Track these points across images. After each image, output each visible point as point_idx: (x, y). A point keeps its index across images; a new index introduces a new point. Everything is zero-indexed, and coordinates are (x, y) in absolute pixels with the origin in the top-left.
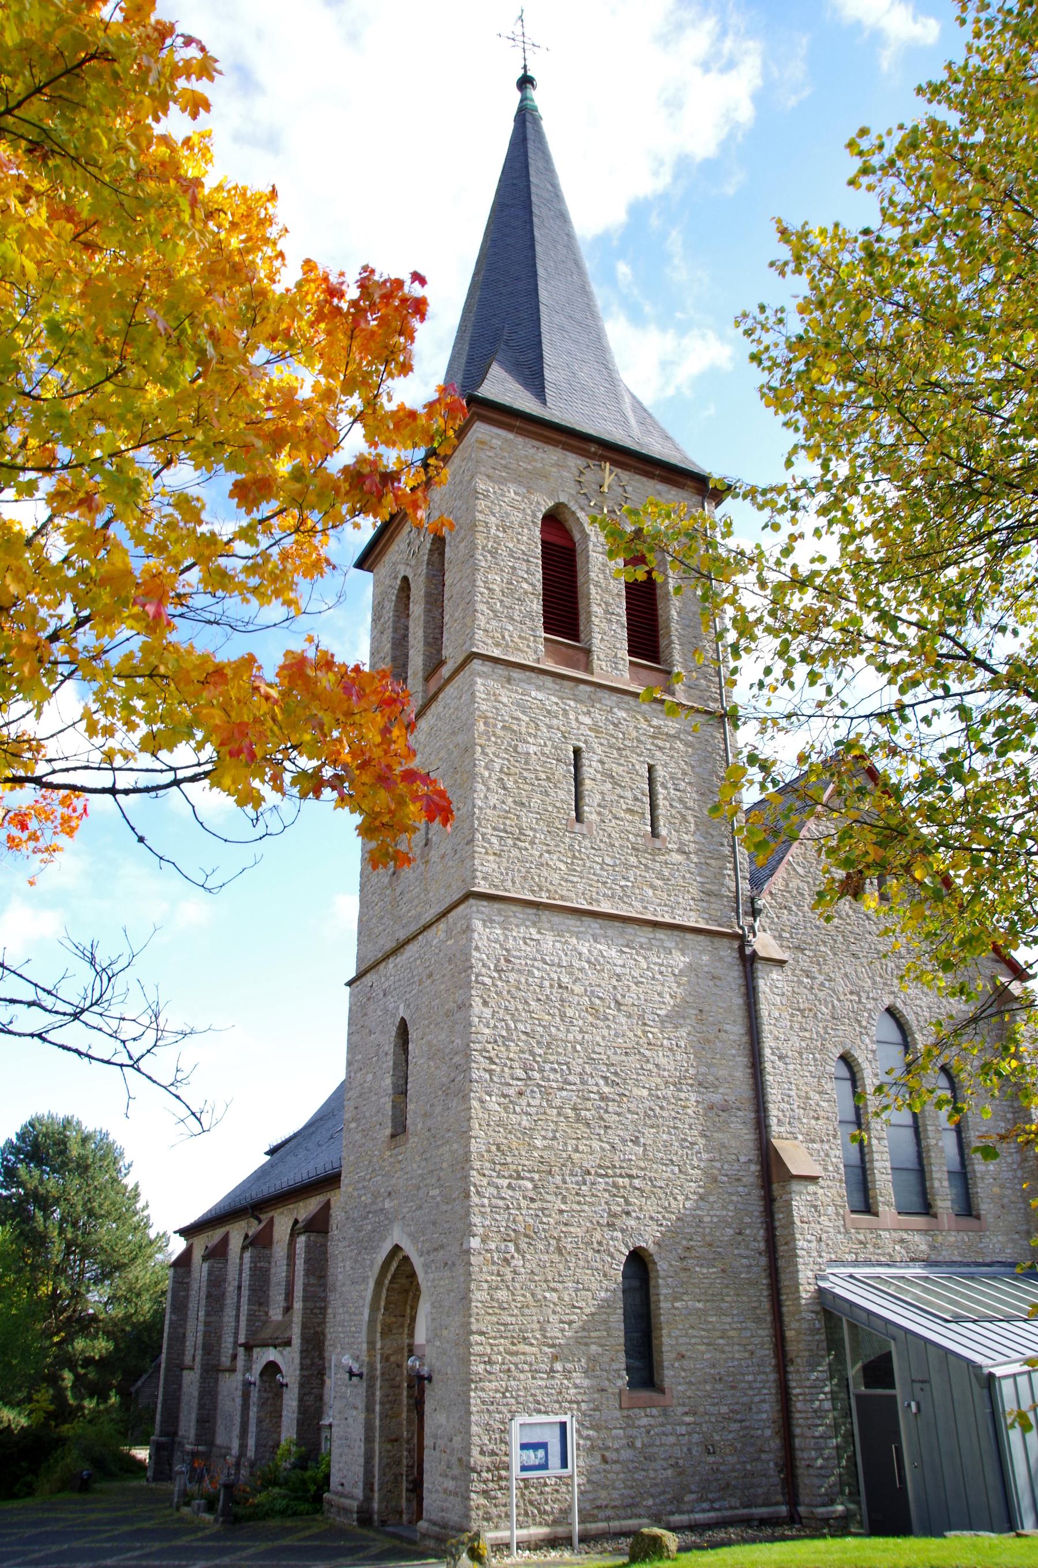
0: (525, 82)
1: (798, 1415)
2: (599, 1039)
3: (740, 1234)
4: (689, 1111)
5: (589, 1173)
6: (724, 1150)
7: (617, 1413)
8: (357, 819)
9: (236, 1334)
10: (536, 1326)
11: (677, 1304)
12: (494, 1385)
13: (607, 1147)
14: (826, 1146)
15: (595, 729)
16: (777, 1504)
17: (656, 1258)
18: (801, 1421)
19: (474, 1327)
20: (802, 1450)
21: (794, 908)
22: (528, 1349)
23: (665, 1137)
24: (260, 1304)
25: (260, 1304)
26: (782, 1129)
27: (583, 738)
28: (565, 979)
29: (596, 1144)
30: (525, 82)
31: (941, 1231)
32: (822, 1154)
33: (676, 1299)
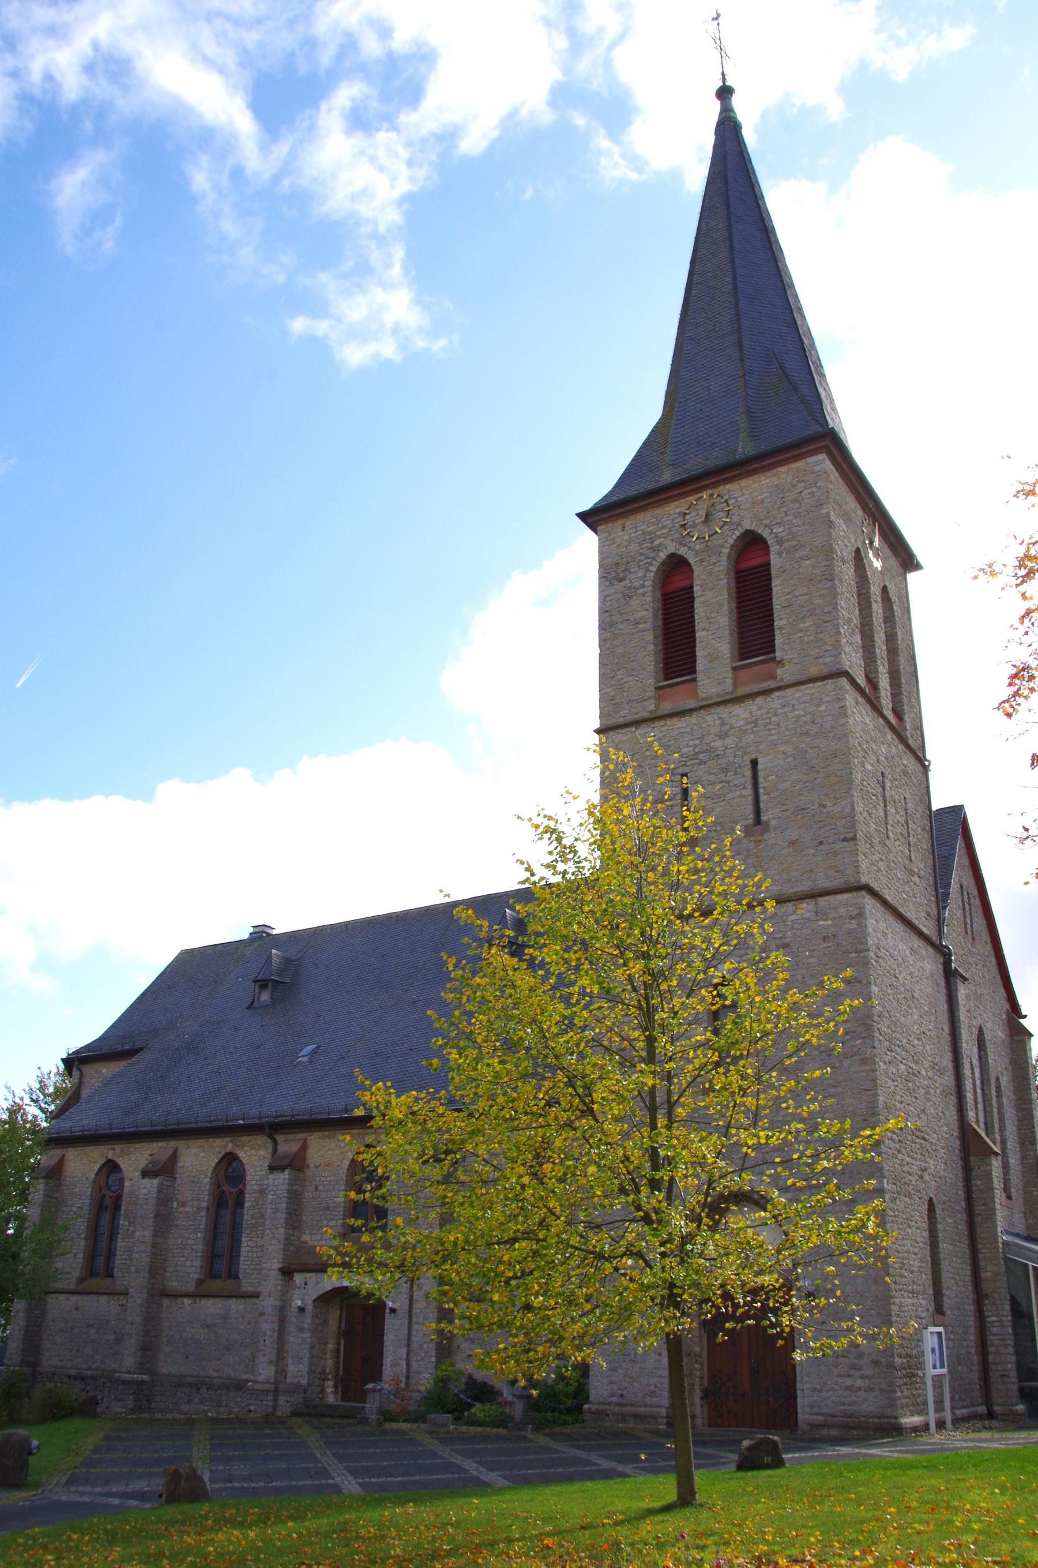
0: (725, 93)
1: (992, 1337)
8: (559, 76)
9: (1006, 1166)
16: (978, 1405)
18: (995, 1342)
20: (997, 1364)
24: (294, 1228)
25: (294, 1228)
30: (725, 93)
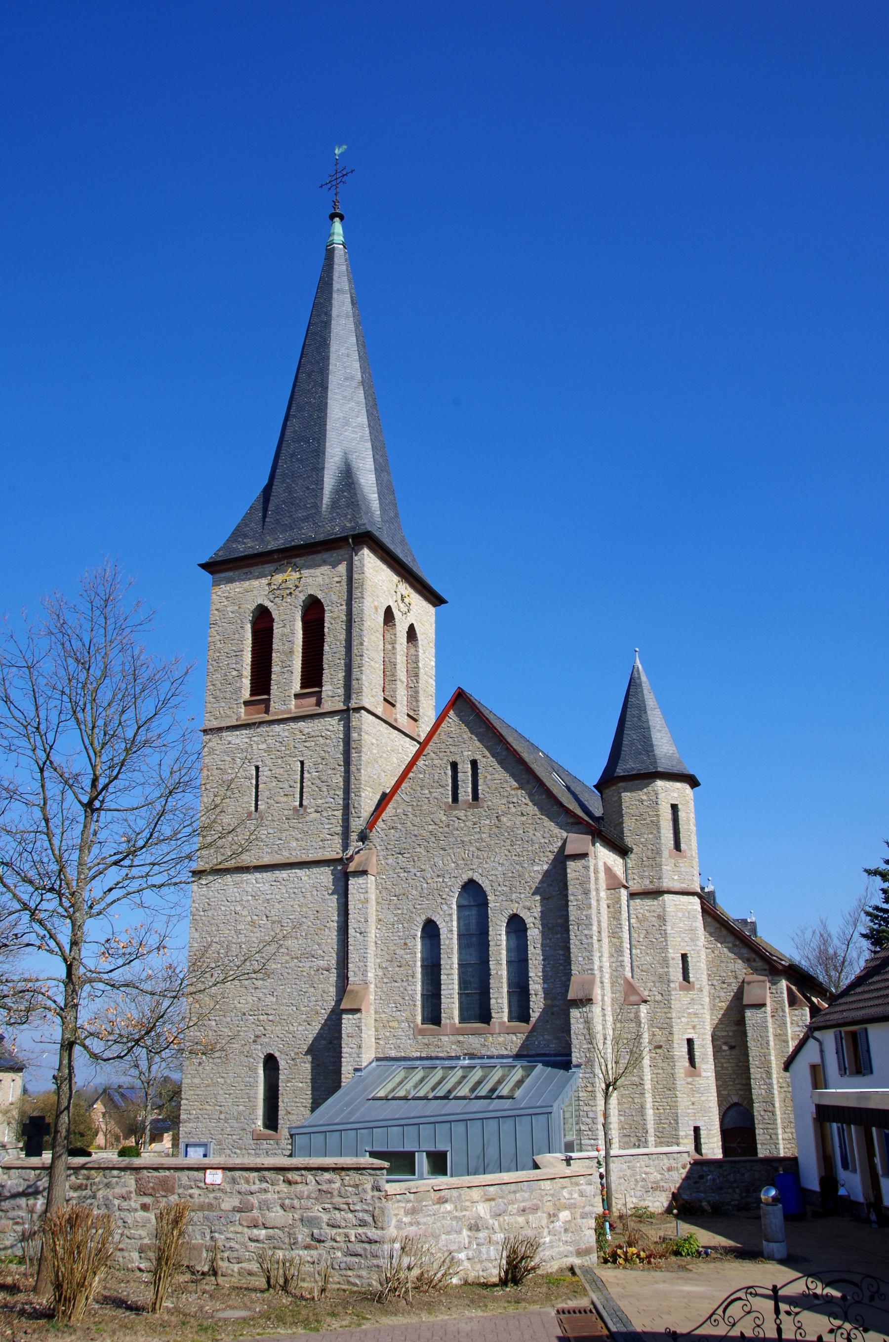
2: (254, 939)
3: (330, 1043)
4: (305, 974)
5: (244, 1014)
6: (325, 995)
7: (252, 1142)
10: (213, 1096)
11: (288, 1085)
12: (191, 1125)
13: (255, 999)
14: (405, 984)
15: (268, 750)
17: (278, 1059)
19: (183, 1097)
21: (399, 826)
22: (208, 1107)
23: (289, 990)
26: (356, 979)
27: (260, 759)
28: (238, 908)
29: (250, 999)
31: (492, 1034)
32: (402, 989)
33: (288, 1081)
